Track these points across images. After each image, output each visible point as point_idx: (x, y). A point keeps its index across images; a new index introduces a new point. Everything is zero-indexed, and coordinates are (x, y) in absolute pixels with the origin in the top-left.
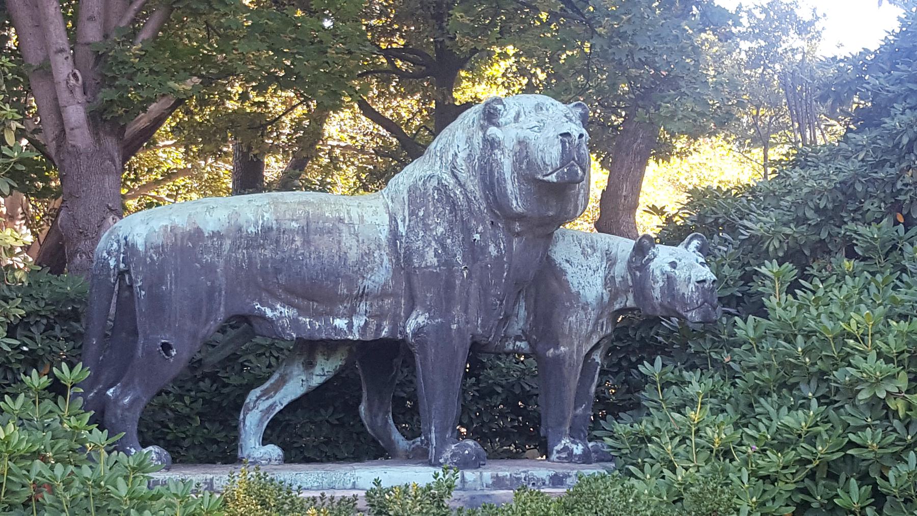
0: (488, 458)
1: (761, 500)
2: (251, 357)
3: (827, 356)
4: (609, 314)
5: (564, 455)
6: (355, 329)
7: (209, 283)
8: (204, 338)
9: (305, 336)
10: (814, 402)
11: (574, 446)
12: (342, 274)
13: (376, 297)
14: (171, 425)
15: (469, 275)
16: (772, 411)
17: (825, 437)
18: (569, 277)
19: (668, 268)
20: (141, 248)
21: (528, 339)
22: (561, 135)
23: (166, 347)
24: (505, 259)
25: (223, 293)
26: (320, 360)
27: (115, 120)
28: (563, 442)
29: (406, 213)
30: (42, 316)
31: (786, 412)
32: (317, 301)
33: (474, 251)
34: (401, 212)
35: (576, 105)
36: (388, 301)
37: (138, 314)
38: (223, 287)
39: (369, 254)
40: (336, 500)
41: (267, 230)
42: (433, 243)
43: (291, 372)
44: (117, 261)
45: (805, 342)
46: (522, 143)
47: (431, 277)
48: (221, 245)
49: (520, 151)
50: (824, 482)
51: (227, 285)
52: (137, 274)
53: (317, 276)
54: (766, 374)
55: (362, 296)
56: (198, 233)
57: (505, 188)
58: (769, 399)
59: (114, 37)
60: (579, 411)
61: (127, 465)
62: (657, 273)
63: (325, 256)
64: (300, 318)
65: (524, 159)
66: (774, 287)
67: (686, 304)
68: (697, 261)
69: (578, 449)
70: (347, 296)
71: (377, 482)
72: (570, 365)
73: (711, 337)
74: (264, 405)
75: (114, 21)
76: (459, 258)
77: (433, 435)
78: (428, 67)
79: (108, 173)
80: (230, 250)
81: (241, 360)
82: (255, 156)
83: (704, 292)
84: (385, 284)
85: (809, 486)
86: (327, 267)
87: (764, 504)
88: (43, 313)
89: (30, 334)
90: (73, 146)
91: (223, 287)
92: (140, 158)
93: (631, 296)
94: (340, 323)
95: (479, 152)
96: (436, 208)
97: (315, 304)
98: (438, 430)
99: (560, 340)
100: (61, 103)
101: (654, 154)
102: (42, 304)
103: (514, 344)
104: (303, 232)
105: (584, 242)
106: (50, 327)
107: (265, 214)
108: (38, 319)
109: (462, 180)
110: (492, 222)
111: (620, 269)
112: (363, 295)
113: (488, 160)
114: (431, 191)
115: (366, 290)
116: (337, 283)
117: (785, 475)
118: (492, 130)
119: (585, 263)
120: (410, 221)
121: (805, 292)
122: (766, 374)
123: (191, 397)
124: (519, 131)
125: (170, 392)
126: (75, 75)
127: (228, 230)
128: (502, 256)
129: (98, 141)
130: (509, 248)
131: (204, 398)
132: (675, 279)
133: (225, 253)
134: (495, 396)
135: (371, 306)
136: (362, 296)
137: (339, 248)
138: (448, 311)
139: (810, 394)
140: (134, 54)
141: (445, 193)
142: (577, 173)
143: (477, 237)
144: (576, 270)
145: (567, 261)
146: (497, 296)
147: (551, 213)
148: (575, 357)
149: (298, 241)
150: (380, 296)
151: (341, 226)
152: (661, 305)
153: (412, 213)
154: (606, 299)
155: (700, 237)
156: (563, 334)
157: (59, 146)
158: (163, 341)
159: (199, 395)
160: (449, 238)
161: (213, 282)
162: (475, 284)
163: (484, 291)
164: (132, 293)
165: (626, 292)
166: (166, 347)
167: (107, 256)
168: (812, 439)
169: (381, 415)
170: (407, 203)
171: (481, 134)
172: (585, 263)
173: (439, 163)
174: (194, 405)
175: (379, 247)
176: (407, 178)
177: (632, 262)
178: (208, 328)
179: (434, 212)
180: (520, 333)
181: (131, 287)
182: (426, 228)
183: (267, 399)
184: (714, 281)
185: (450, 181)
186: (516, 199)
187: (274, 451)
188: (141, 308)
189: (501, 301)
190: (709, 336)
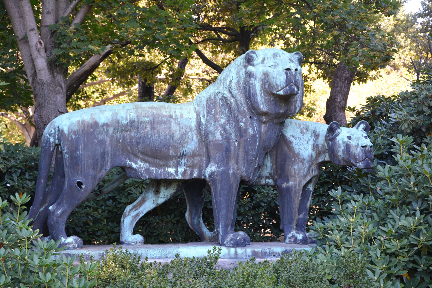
0: (252, 241)
1: (387, 267)
2: (132, 188)
3: (427, 187)
4: (316, 164)
5: (292, 240)
6: (179, 173)
7: (102, 150)
8: (100, 178)
9: (153, 177)
10: (418, 213)
11: (298, 235)
12: (172, 145)
13: (190, 156)
14: (91, 224)
15: (239, 145)
16: (396, 218)
17: (425, 231)
18: (294, 145)
19: (346, 140)
20: (66, 132)
21: (273, 178)
22: (286, 69)
23: (80, 184)
24: (257, 136)
25: (109, 155)
26: (163, 189)
27: (61, 65)
28: (292, 233)
29: (205, 112)
30: (18, 168)
31: (404, 218)
32: (159, 159)
34: (202, 112)
35: (296, 54)
36: (196, 159)
37: (65, 167)
38: (110, 152)
39: (186, 134)
40: (162, 264)
41: (132, 122)
42: (219, 128)
43: (148, 196)
44: (54, 139)
45: (415, 179)
46: (266, 74)
47: (218, 146)
48: (108, 130)
49: (265, 79)
50: (425, 257)
51: (111, 151)
52: (64, 145)
53: (159, 146)
54: (394, 197)
55: (182, 156)
56: (96, 124)
57: (257, 99)
58: (395, 211)
59: (60, 22)
60: (301, 216)
61: (43, 247)
62: (341, 142)
63: (163, 135)
64: (150, 168)
65: (266, 82)
66: (400, 149)
67: (356, 159)
68: (363, 135)
69: (300, 237)
70: (174, 156)
71: (178, 256)
72: (295, 191)
73: (371, 176)
74: (133, 214)
75: (61, 14)
76: (233, 136)
78: (235, 36)
79: (59, 93)
80: (113, 133)
81: (127, 190)
82: (149, 84)
83: (366, 152)
84: (194, 150)
85: (416, 259)
86: (164, 141)
87: (389, 269)
88: (19, 166)
89: (11, 178)
90: (40, 79)
91: (110, 152)
92: (102, 86)
93: (327, 155)
94: (172, 170)
95: (243, 79)
96: (221, 109)
97: (158, 161)
98: (223, 226)
99: (290, 178)
100: (34, 57)
101: (357, 79)
102: (19, 162)
103: (266, 180)
104: (151, 123)
105: (302, 126)
106: (22, 174)
107: (131, 114)
108: (16, 170)
110: (250, 117)
111: (321, 140)
112: (183, 156)
113: (248, 83)
114: (218, 101)
115: (184, 153)
116: (169, 149)
117: (402, 253)
118: (250, 68)
120: (207, 116)
121: (416, 152)
122: (394, 197)
123: (102, 209)
124: (264, 68)
125: (91, 207)
126: (40, 43)
127: (111, 122)
128: (256, 134)
129: (53, 76)
130: (260, 131)
131: (108, 210)
132: (350, 145)
133: (111, 134)
134: (261, 208)
135: (187, 161)
136: (182, 156)
137: (170, 131)
138: (228, 163)
139: (418, 208)
140: (70, 31)
141: (226, 101)
142: (294, 90)
143: (242, 124)
144: (297, 141)
145: (293, 136)
147: (282, 111)
148: (297, 187)
149: (149, 127)
150: (192, 156)
151: (171, 119)
152: (343, 159)
153: (209, 112)
154: (314, 156)
155: (365, 122)
156: (291, 175)
157: (33, 80)
158: (78, 181)
159: (106, 208)
160: (227, 125)
161: (104, 150)
163: (246, 152)
164: (62, 155)
165: (325, 152)
166: (80, 184)
167: (49, 136)
168: (417, 233)
169: (196, 219)
170: (205, 107)
171: (244, 70)
173: (222, 86)
174: (103, 213)
175: (191, 130)
176: (206, 94)
177: (327, 137)
178: (101, 173)
179: (220, 112)
180: (268, 175)
181: (61, 153)
182: (216, 120)
183: (135, 210)
184: (371, 146)
185: (227, 94)
186: (263, 104)
187: (139, 238)
189: (256, 158)
190: (369, 176)
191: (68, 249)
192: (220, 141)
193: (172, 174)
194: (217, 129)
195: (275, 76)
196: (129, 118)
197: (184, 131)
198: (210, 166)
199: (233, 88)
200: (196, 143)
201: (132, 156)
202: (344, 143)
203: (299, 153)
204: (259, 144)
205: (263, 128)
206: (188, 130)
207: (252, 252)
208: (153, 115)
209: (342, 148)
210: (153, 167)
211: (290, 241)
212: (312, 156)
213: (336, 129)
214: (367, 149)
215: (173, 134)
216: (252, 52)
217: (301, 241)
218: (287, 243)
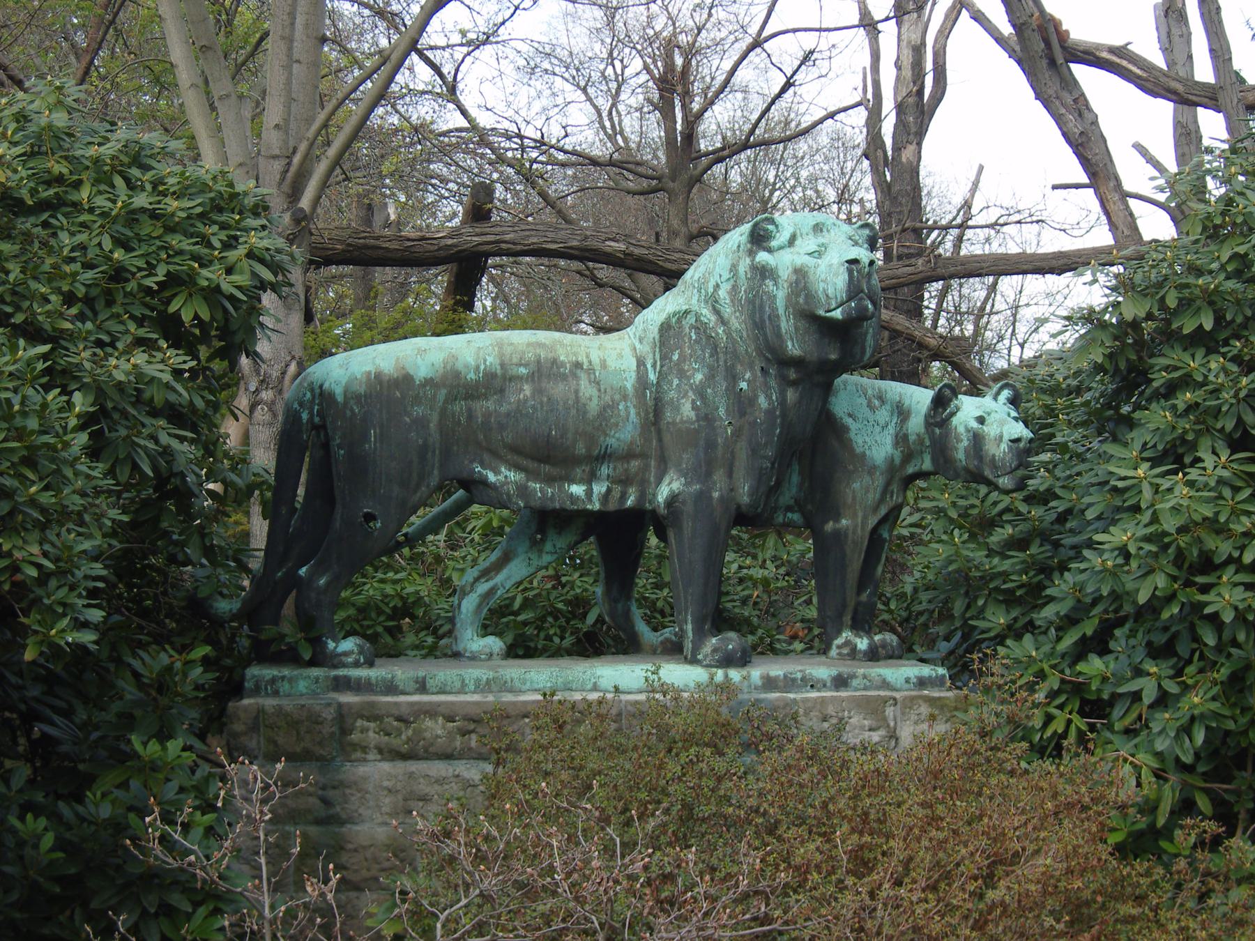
5: (845, 651)
7: (420, 442)
9: (536, 504)
11: (858, 641)
18: (852, 435)
19: (974, 425)
20: (340, 399)
22: (847, 262)
23: (370, 517)
28: (844, 635)
34: (651, 356)
36: (635, 464)
38: (437, 445)
39: (613, 406)
41: (490, 376)
42: (690, 394)
49: (797, 282)
62: (961, 429)
68: (1009, 415)
69: (862, 644)
76: (722, 412)
80: (446, 402)
84: (631, 443)
94: (577, 490)
96: (694, 351)
105: (870, 392)
109: (726, 316)
111: (916, 424)
114: (687, 330)
118: (763, 256)
120: (662, 366)
124: (795, 257)
128: (774, 409)
130: (782, 401)
132: (984, 437)
135: (614, 469)
138: (709, 474)
142: (866, 309)
143: (744, 385)
145: (850, 415)
147: (833, 357)
154: (897, 461)
175: (625, 397)
178: (418, 494)
180: (792, 502)
182: (682, 374)
184: (1031, 441)
185: (707, 315)
187: (494, 643)
191: (344, 666)
192: (692, 423)
193: (578, 498)
194: (686, 395)
195: (823, 277)
196: (482, 367)
197: (608, 398)
198: (666, 480)
199: (722, 302)
200: (635, 427)
201: (486, 456)
202: (968, 430)
203: (864, 455)
204: (781, 432)
205: (791, 395)
206: (617, 397)
207: (762, 677)
208: (539, 362)
209: (965, 443)
210: (536, 480)
211: (839, 654)
212: (893, 460)
213: (951, 400)
214: (1022, 445)
215: (584, 405)
216: (767, 219)
217: (865, 653)
218: (833, 658)
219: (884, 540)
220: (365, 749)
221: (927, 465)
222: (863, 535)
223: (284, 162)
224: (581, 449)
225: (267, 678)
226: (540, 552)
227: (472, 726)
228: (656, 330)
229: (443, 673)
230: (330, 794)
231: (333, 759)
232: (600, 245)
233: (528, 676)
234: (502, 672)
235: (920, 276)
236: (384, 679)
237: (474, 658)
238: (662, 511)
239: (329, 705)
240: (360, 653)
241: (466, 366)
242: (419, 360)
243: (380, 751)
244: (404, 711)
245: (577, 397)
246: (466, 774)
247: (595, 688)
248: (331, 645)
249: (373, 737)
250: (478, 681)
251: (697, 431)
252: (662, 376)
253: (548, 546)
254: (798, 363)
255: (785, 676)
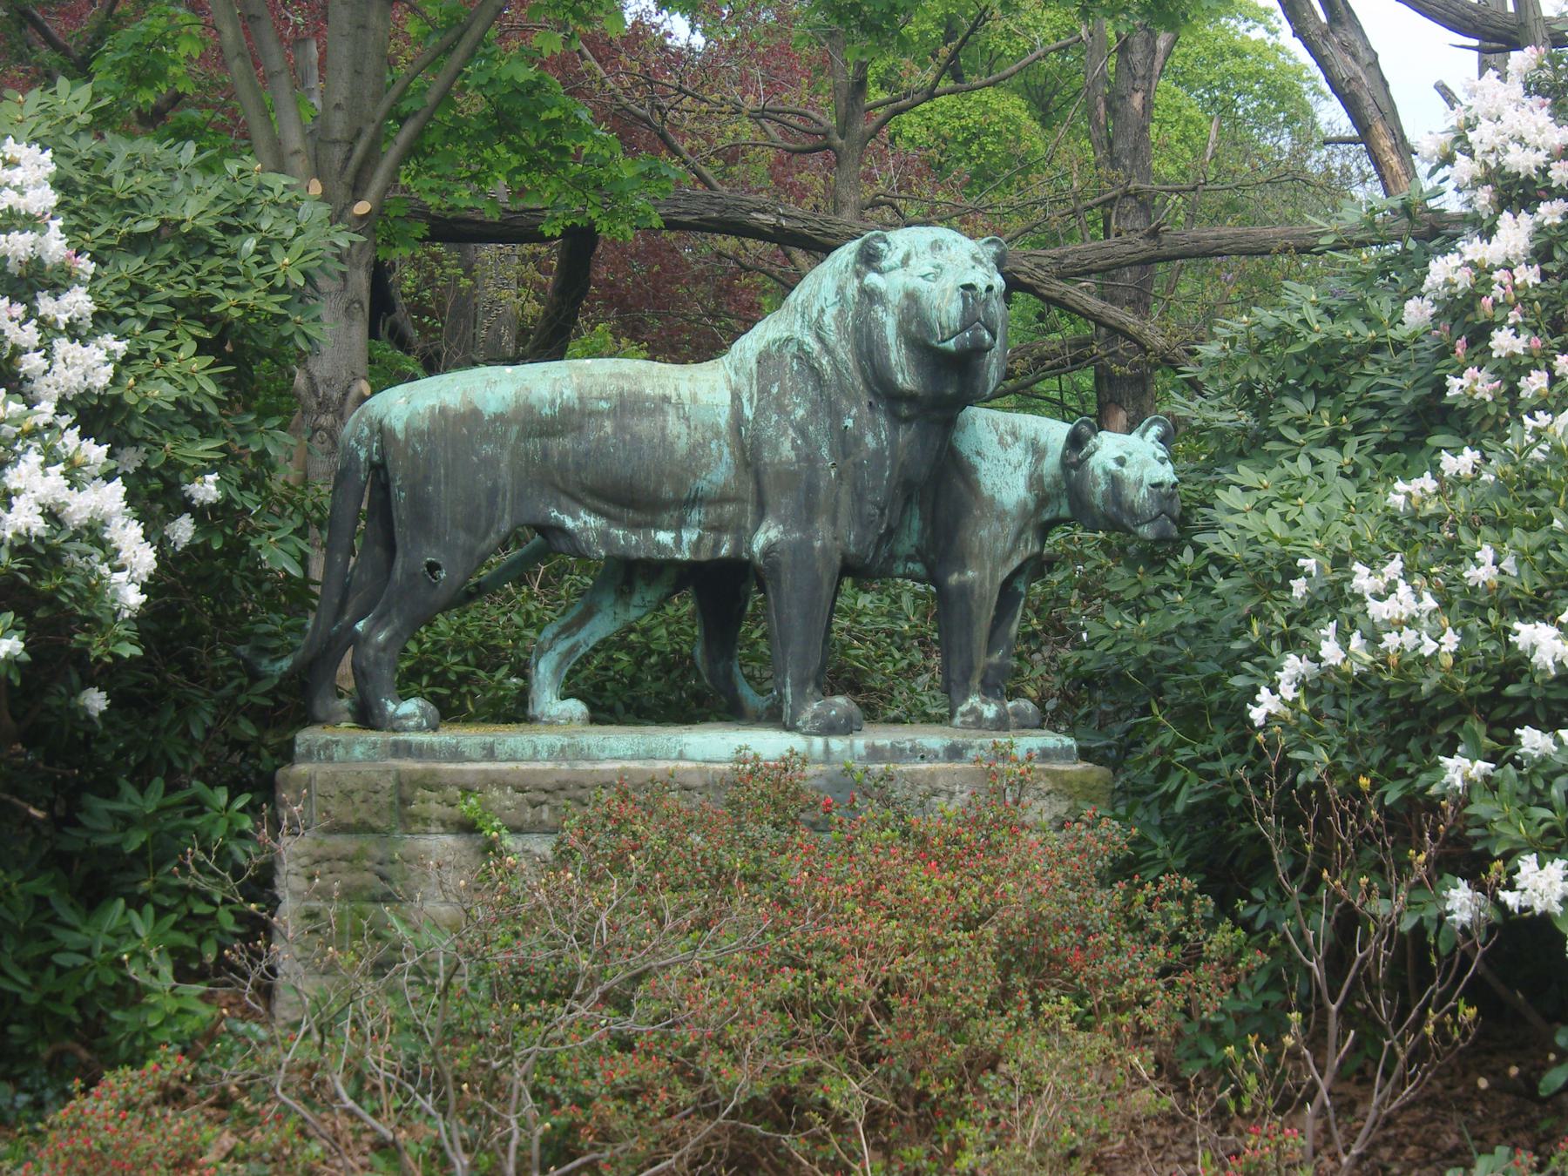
5: (970, 719)
6: (685, 546)
7: (489, 484)
11: (985, 708)
15: (839, 475)
20: (401, 436)
21: (924, 561)
23: (433, 567)
33: (845, 443)
34: (747, 389)
36: (729, 509)
38: (509, 487)
39: (704, 444)
41: (567, 411)
42: (790, 431)
47: (787, 478)
57: (888, 358)
62: (1099, 472)
69: (990, 711)
74: (563, 646)
76: (825, 452)
77: (789, 690)
94: (665, 537)
105: (1002, 427)
109: (831, 344)
111: (1051, 463)
112: (695, 501)
118: (873, 279)
119: (1002, 456)
128: (883, 450)
130: (893, 442)
135: (707, 514)
143: (849, 423)
146: (875, 504)
147: (950, 391)
153: (763, 390)
154: (1031, 506)
162: (845, 488)
163: (859, 496)
166: (433, 567)
171: (856, 282)
172: (1002, 456)
175: (718, 435)
180: (913, 551)
182: (782, 410)
184: (1174, 486)
187: (576, 707)
188: (401, 512)
191: (405, 730)
192: (792, 464)
193: (665, 546)
194: (785, 433)
197: (698, 436)
198: (763, 527)
201: (564, 500)
202: (1106, 472)
206: (709, 435)
207: (866, 747)
208: (621, 394)
209: (1103, 487)
216: (877, 236)
217: (992, 721)
219: (1020, 595)
220: (426, 821)
221: (1065, 511)
222: (990, 592)
223: (345, 148)
224: (667, 492)
225: (321, 742)
226: (627, 605)
227: (544, 797)
228: (754, 361)
229: (512, 738)
230: (387, 869)
231: (392, 830)
232: (745, 218)
233: (606, 743)
234: (578, 738)
235: (1141, 256)
236: (448, 746)
237: (551, 723)
238: (759, 561)
239: (388, 772)
240: (423, 716)
241: (541, 400)
242: (489, 394)
243: (443, 824)
244: (469, 779)
245: (664, 435)
246: (537, 850)
247: (681, 756)
248: (391, 707)
249: (435, 809)
250: (551, 749)
251: (795, 474)
252: (760, 412)
253: (636, 599)
254: (910, 398)
255: (893, 745)
